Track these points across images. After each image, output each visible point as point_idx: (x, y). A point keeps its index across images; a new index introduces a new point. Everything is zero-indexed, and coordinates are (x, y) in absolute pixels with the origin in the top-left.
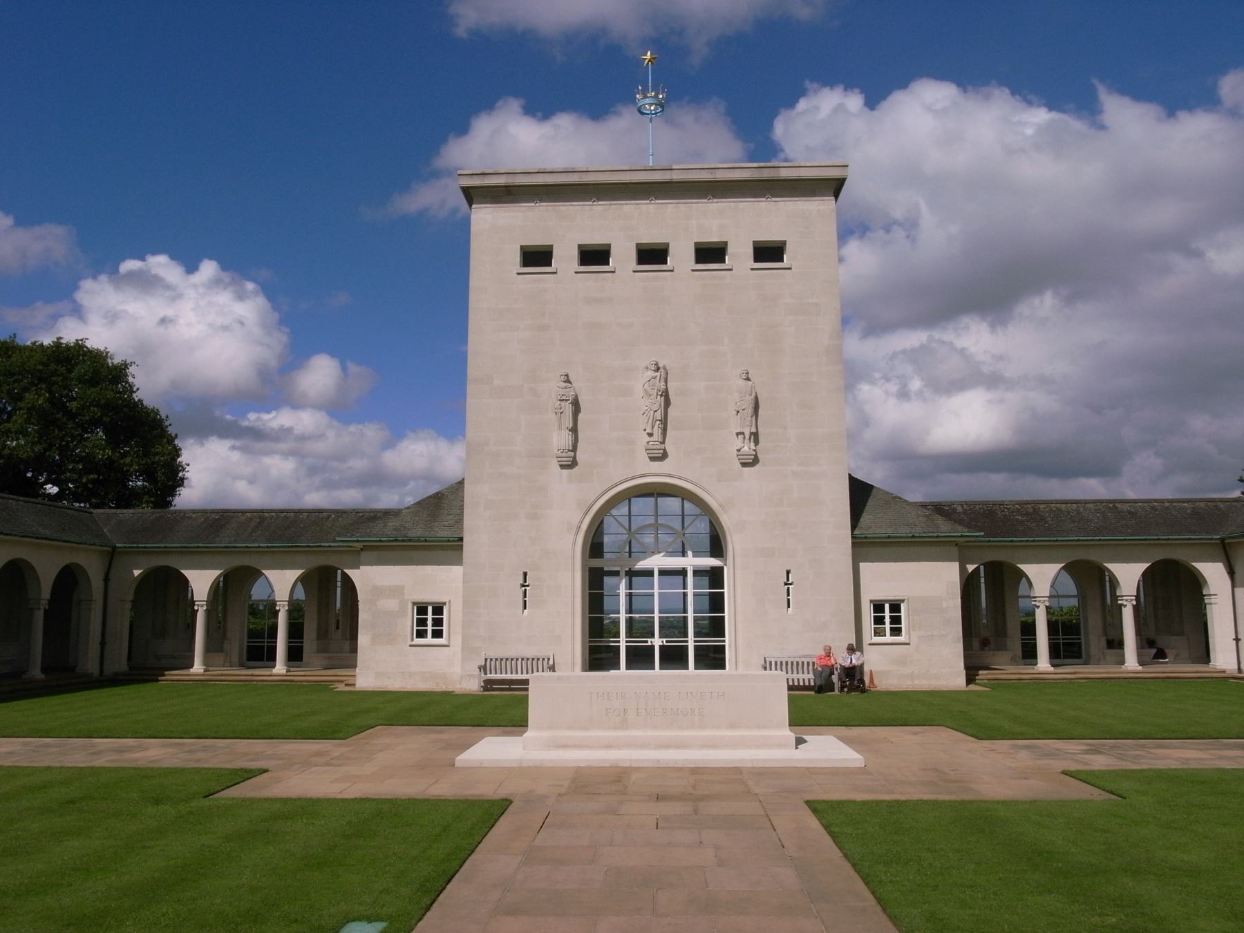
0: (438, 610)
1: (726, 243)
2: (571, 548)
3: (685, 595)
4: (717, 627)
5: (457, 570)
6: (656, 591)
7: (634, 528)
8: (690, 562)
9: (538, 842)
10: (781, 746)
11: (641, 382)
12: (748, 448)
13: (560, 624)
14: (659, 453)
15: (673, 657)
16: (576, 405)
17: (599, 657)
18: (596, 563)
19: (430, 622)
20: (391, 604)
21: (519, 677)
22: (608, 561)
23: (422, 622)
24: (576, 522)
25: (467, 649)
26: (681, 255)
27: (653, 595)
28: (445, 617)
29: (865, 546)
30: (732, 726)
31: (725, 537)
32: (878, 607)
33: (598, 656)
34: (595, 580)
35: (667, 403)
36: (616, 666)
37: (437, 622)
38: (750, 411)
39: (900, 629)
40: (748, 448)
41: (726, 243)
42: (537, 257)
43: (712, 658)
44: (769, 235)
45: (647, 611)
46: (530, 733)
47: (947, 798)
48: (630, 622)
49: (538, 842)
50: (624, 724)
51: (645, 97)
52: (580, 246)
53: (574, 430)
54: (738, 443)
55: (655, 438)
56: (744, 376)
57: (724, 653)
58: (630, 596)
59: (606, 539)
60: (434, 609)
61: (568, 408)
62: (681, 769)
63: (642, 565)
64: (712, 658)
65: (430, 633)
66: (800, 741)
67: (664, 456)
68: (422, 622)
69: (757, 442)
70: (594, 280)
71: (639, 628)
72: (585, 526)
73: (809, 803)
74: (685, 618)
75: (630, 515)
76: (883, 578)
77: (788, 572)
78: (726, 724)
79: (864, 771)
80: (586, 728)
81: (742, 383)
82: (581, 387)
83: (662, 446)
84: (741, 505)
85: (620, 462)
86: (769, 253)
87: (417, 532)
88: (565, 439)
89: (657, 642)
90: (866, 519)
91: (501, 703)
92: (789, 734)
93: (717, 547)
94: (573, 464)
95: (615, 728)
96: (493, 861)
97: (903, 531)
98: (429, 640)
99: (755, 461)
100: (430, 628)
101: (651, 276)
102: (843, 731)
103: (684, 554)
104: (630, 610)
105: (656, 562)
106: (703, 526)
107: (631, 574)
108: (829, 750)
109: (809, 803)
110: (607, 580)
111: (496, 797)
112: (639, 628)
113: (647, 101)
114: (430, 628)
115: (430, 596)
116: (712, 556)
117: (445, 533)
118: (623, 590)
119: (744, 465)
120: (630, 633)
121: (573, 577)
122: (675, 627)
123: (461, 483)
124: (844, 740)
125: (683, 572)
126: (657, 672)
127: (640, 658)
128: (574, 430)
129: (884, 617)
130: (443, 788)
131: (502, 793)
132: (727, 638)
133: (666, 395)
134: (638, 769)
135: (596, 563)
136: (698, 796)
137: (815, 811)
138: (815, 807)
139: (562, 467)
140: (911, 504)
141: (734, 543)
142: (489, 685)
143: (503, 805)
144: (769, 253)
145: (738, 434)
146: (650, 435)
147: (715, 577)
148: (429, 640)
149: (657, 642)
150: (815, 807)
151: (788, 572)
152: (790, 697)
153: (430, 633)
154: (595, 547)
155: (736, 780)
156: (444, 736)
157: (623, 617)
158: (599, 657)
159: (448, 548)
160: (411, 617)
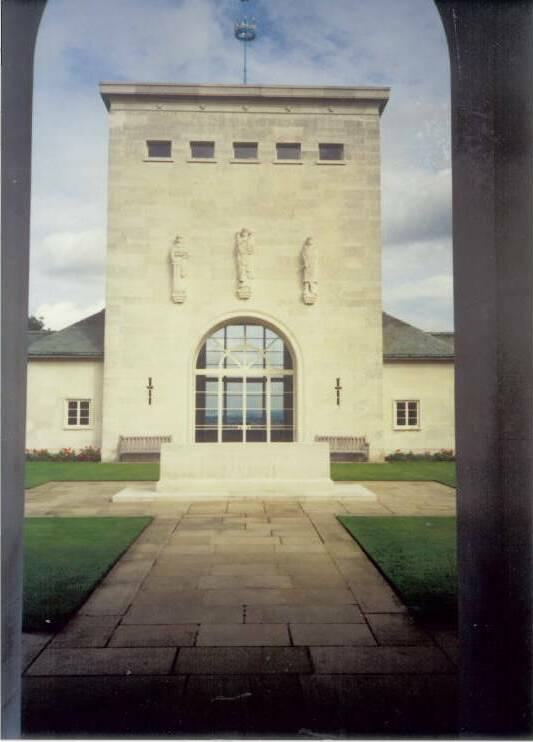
6: (245, 392)
13: (175, 415)
18: (201, 372)
36: (216, 440)
39: (87, 420)
45: (407, 413)
59: (208, 354)
60: (82, 404)
65: (78, 421)
78: (295, 473)
89: (244, 427)
91: (141, 463)
100: (79, 417)
102: (367, 483)
106: (279, 345)
110: (208, 384)
114: (79, 417)
118: (220, 392)
122: (257, 419)
124: (369, 488)
126: (244, 447)
127: (232, 436)
129: (404, 412)
135: (201, 372)
143: (151, 520)
149: (244, 427)
153: (78, 421)
155: (295, 509)
157: (220, 409)
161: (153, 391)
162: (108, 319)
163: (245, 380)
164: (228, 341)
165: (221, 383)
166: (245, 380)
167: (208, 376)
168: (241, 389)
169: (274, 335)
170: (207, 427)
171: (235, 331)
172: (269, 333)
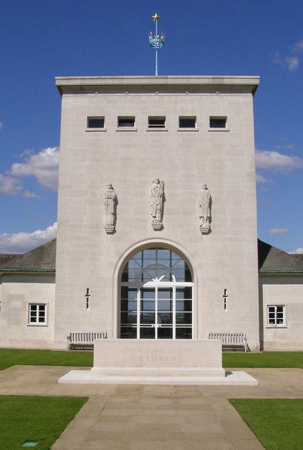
0: (42, 307)
1: (195, 117)
2: (113, 276)
3: (171, 302)
4: (187, 318)
5: (52, 286)
6: (156, 299)
7: (145, 266)
8: (174, 284)
9: (102, 414)
10: (219, 375)
11: (150, 190)
12: (206, 225)
14: (159, 227)
15: (165, 333)
16: (116, 201)
17: (126, 331)
18: (125, 284)
19: (38, 314)
20: (18, 304)
21: (88, 343)
22: (131, 283)
23: (34, 314)
24: (115, 262)
25: (58, 329)
26: (172, 123)
27: (154, 301)
28: (46, 311)
29: (265, 277)
30: (195, 366)
31: (192, 271)
32: (272, 309)
33: (125, 333)
34: (124, 293)
35: (164, 200)
37: (42, 314)
38: (207, 205)
40: (206, 225)
41: (195, 117)
42: (96, 123)
43: (185, 333)
44: (218, 113)
46: (93, 369)
47: (294, 398)
48: (142, 316)
49: (102, 414)
50: (141, 365)
51: (154, 38)
52: (119, 117)
53: (115, 214)
54: (201, 222)
55: (157, 219)
56: (204, 187)
57: (191, 332)
58: (142, 302)
61: (111, 203)
62: (169, 386)
63: (148, 285)
64: (185, 333)
65: (38, 320)
66: (227, 374)
67: (162, 228)
68: (34, 314)
69: (210, 222)
70: (125, 135)
71: (148, 319)
72: (119, 265)
73: (231, 400)
74: (171, 314)
75: (171, 260)
76: (276, 294)
77: (225, 290)
78: (192, 365)
79: (258, 387)
80: (123, 366)
81: (202, 190)
82: (118, 191)
83: (161, 223)
84: (200, 254)
85: (139, 232)
86: (218, 122)
87: (31, 267)
88: (110, 219)
89: (156, 326)
90: (266, 264)
91: (80, 355)
92: (223, 371)
93: (188, 276)
94: (114, 231)
95: (136, 366)
96: (82, 422)
97: (284, 269)
98: (37, 323)
99: (210, 231)
100: (38, 317)
101: (157, 134)
102: (250, 370)
103: (171, 280)
104: (142, 309)
105: (156, 283)
106: (182, 263)
107: (143, 290)
108: (242, 378)
109: (231, 400)
111: (81, 396)
112: (148, 319)
113: (155, 40)
114: (38, 317)
115: (38, 300)
116: (186, 281)
117: (45, 267)
118: (139, 299)
119: (203, 234)
120: (142, 321)
121: (113, 292)
123: (54, 241)
124: (249, 373)
125: (170, 290)
127: (148, 333)
128: (115, 214)
130: (55, 392)
131: (84, 394)
132: (193, 324)
133: (163, 196)
134: (148, 385)
135: (125, 284)
136: (177, 396)
137: (233, 404)
138: (235, 403)
139: (108, 233)
140: (289, 255)
141: (197, 274)
142: (73, 347)
144: (218, 122)
145: (200, 217)
146: (155, 217)
147: (187, 292)
148: (37, 323)
149: (156, 326)
150: (235, 403)
151: (225, 290)
152: (223, 354)
153: (38, 320)
154: (124, 276)
156: (50, 370)
158: (126, 331)
159: (48, 276)
160: (28, 311)
161: (165, 203)
162: (59, 245)
163: (156, 290)
164: (144, 261)
165: (139, 293)
166: (156, 290)
167: (129, 287)
168: (178, 280)
169: (179, 257)
170: (128, 325)
171: (149, 253)
172: (175, 256)
